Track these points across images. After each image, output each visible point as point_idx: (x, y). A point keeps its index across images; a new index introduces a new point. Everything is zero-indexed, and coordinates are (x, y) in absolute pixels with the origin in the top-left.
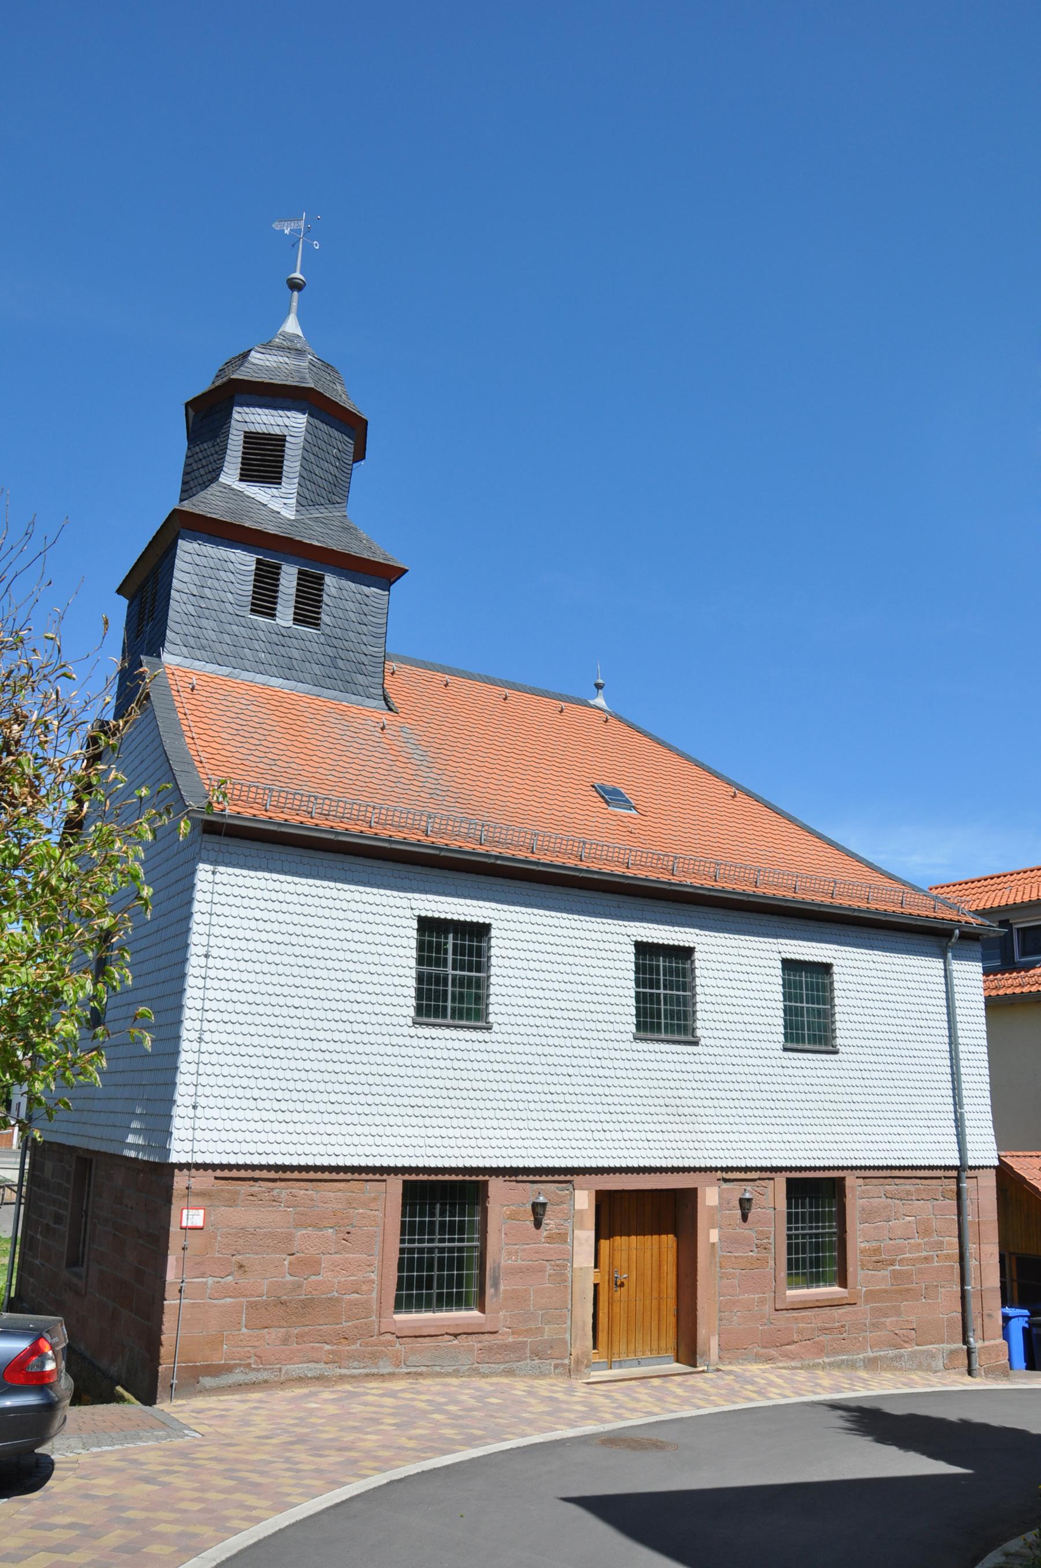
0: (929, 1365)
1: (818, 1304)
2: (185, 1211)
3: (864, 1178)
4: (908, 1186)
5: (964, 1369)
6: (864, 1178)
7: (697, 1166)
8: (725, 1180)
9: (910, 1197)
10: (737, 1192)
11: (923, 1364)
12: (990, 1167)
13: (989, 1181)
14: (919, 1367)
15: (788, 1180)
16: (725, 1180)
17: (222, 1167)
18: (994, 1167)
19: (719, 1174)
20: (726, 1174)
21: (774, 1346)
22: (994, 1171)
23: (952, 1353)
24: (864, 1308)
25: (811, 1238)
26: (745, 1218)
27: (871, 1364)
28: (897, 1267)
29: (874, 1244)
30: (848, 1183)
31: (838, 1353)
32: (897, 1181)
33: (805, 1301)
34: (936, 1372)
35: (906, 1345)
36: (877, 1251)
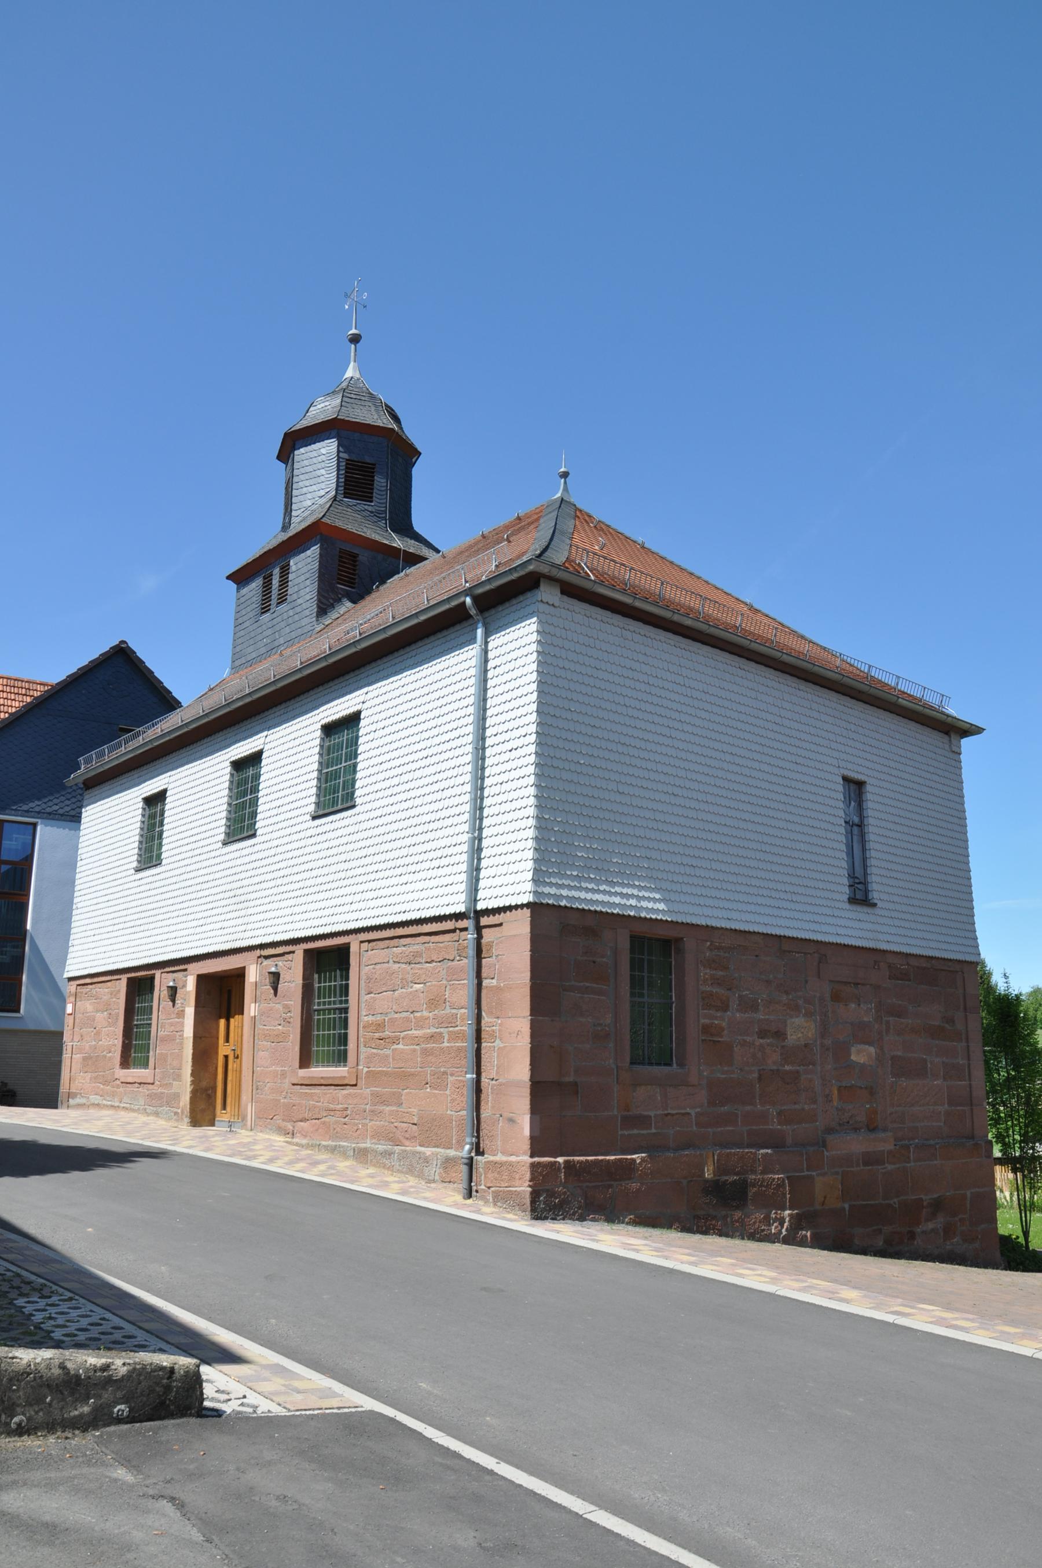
0: (422, 1171)
1: (323, 1082)
2: (206, 1404)
3: (369, 941)
4: (415, 946)
5: (463, 1185)
6: (369, 941)
7: (501, 905)
8: (267, 957)
9: (418, 960)
10: (271, 966)
11: (414, 1167)
12: (522, 906)
13: (520, 926)
14: (411, 1171)
15: (306, 951)
16: (267, 957)
17: (262, 946)
18: (528, 905)
19: (258, 952)
20: (264, 949)
21: (285, 1120)
22: (527, 912)
23: (448, 1162)
24: (365, 1091)
25: (329, 1014)
26: (276, 994)
27: (362, 1155)
28: (400, 1046)
29: (379, 1018)
30: (354, 948)
31: (341, 1139)
32: (403, 941)
33: (313, 1077)
34: (429, 1182)
35: (407, 1143)
36: (380, 1026)
